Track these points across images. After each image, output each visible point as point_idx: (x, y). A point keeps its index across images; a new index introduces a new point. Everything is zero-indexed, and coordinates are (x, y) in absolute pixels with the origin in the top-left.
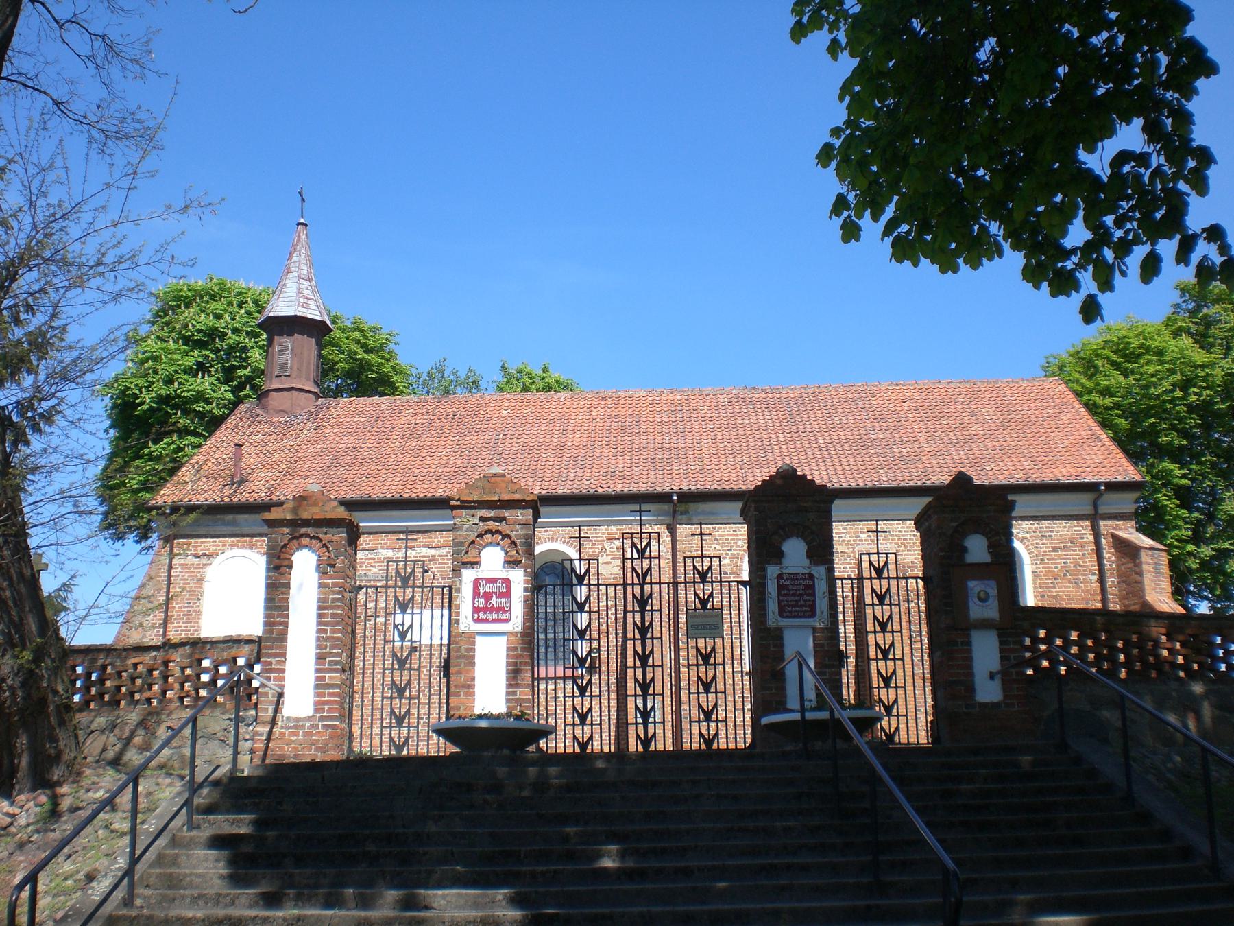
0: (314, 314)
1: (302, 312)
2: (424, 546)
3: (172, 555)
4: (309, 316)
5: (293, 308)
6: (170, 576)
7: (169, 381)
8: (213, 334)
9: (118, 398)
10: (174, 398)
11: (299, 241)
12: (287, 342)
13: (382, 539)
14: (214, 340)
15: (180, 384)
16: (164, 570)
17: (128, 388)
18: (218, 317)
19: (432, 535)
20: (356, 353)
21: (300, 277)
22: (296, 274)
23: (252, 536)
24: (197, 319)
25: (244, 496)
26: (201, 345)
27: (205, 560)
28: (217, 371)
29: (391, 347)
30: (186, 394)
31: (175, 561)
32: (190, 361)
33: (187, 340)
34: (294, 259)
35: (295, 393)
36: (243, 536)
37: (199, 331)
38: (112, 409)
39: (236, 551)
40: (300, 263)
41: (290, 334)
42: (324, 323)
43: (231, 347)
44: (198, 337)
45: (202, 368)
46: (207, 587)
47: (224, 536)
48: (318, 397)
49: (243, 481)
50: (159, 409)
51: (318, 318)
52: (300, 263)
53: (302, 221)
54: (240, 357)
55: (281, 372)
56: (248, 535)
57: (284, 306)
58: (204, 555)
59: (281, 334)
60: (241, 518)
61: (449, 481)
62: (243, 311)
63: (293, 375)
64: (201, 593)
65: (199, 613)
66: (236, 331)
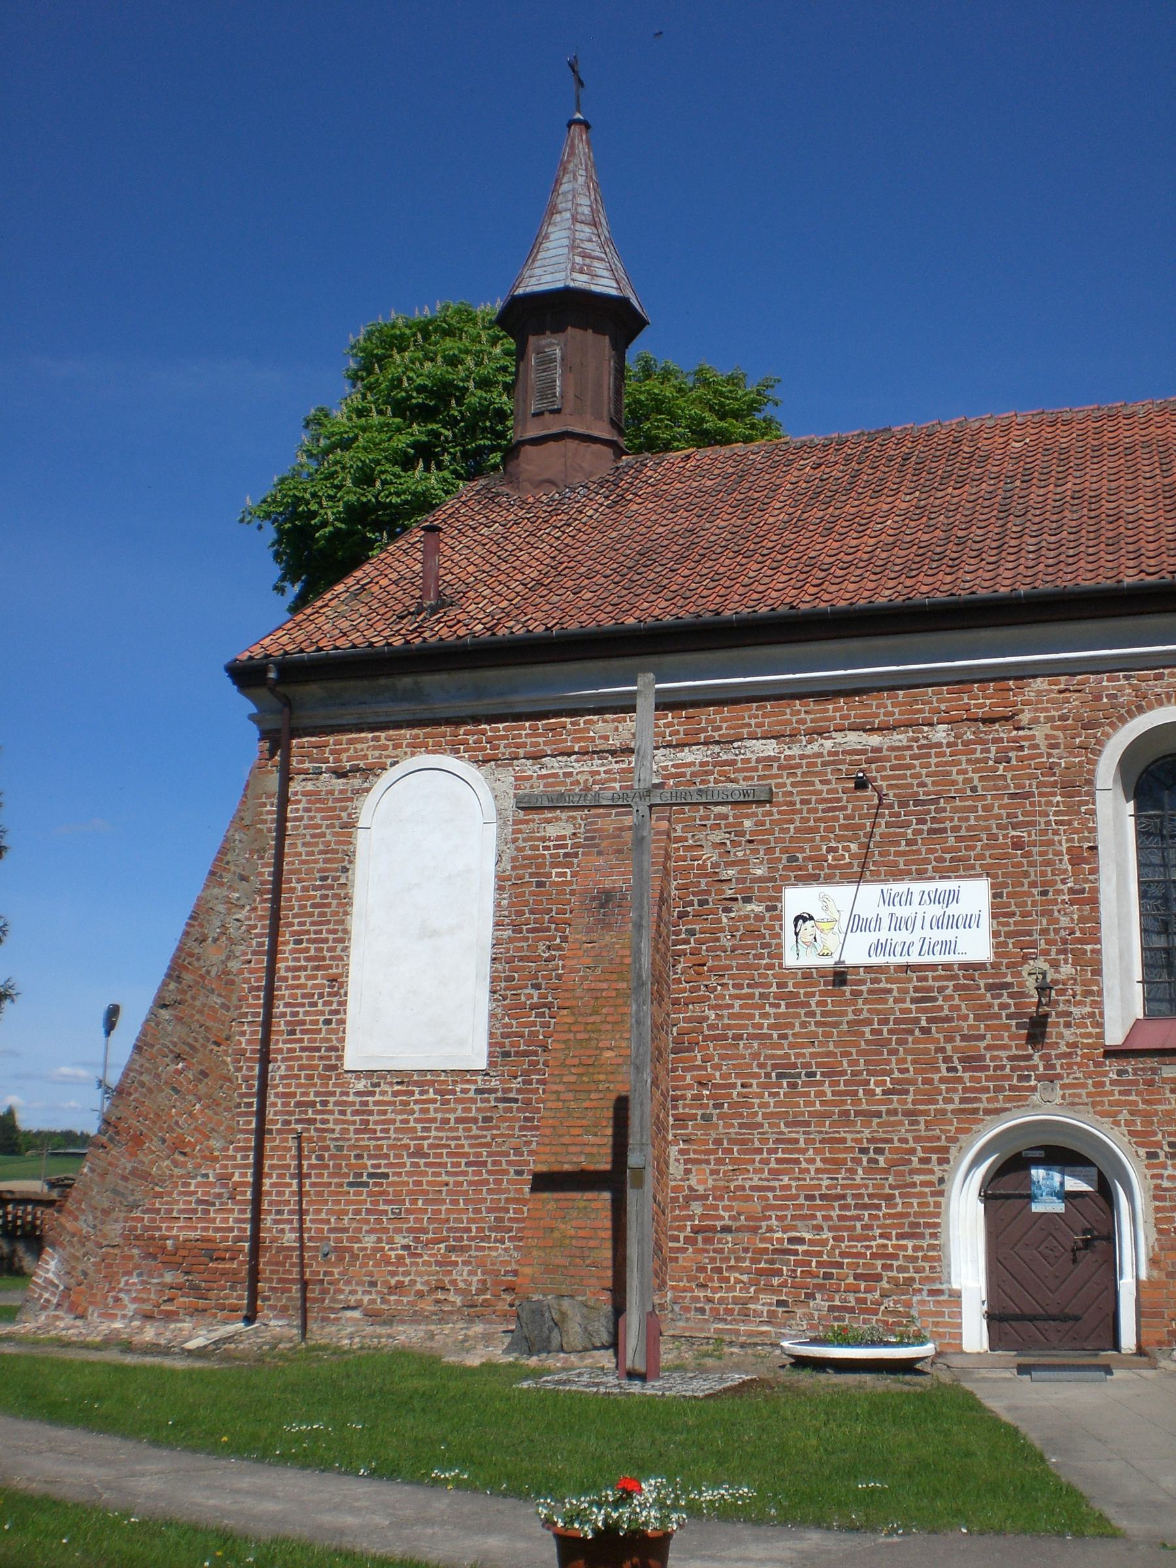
0: (605, 285)
1: (581, 281)
2: (854, 728)
3: (286, 778)
4: (594, 288)
5: (562, 275)
6: (282, 819)
7: (365, 478)
8: (444, 391)
9: (285, 521)
10: (376, 511)
11: (572, 153)
12: (554, 346)
13: (751, 715)
14: (447, 406)
15: (384, 483)
16: (271, 808)
17: (298, 500)
18: (453, 361)
19: (872, 701)
20: (703, 420)
21: (574, 219)
22: (568, 215)
23: (457, 722)
24: (417, 370)
25: (438, 632)
26: (425, 414)
27: (356, 782)
28: (454, 459)
29: (769, 411)
30: (395, 500)
31: (294, 787)
32: (401, 442)
33: (401, 408)
34: (565, 187)
35: (572, 445)
36: (436, 722)
37: (421, 389)
38: (278, 542)
39: (425, 759)
40: (577, 191)
41: (559, 329)
42: (624, 302)
43: (475, 412)
44: (418, 399)
45: (426, 452)
46: (362, 840)
47: (398, 726)
48: (619, 452)
49: (442, 603)
50: (350, 533)
51: (614, 292)
52: (577, 191)
53: (578, 116)
54: (492, 430)
55: (543, 406)
56: (448, 722)
57: (548, 273)
58: (356, 769)
59: (540, 332)
60: (429, 681)
61: (907, 571)
62: (498, 350)
63: (567, 410)
64: (350, 856)
65: (345, 902)
66: (485, 383)
